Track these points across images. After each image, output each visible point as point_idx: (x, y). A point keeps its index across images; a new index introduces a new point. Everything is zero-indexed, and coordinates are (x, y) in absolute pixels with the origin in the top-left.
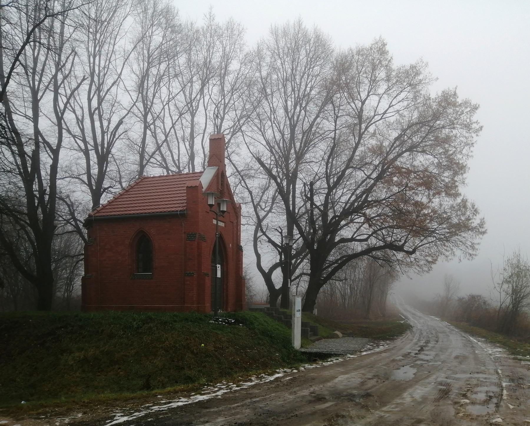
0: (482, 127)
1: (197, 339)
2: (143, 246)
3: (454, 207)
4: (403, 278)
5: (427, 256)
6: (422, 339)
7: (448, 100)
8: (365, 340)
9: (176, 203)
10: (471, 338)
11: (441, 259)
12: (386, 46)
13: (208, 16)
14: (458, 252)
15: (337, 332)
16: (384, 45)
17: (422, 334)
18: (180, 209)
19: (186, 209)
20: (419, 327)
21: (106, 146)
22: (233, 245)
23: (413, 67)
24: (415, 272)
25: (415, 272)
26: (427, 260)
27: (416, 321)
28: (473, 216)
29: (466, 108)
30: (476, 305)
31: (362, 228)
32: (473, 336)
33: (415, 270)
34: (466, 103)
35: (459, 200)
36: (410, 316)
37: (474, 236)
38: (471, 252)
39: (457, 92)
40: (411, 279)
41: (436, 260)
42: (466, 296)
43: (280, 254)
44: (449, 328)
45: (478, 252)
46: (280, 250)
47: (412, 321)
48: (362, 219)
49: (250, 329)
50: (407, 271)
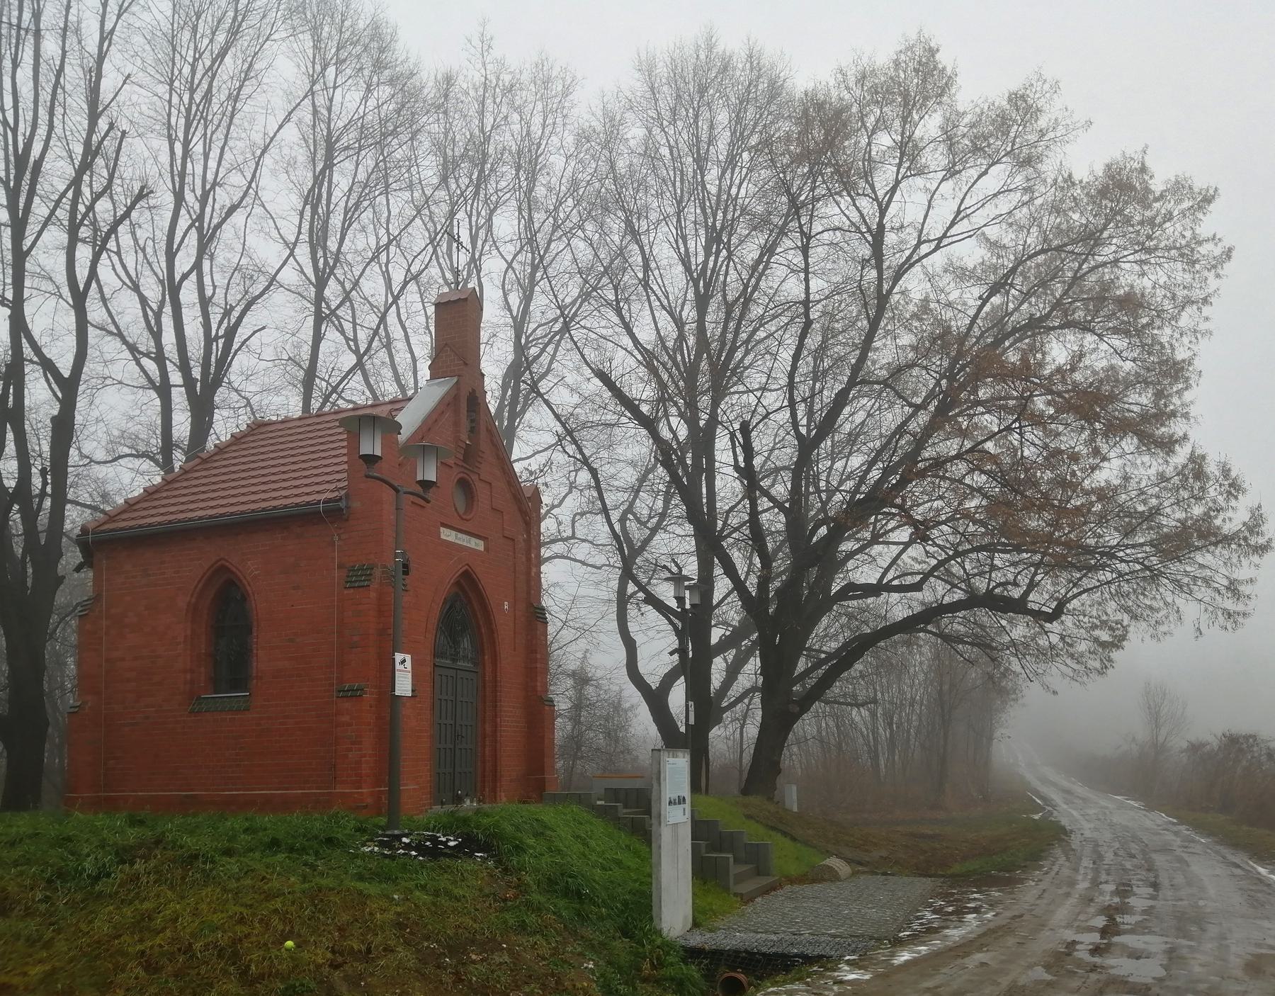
0: (1230, 250)
1: (275, 921)
2: (227, 614)
3: (1168, 480)
4: (1032, 693)
5: (1094, 627)
6: (1103, 877)
7: (1121, 188)
8: (922, 885)
9: (322, 482)
10: (1261, 870)
11: (1137, 634)
12: (938, 56)
13: (476, 42)
14: (1190, 610)
15: (834, 862)
16: (932, 52)
17: (1101, 857)
18: (323, 497)
19: (347, 495)
20: (1088, 834)
21: (212, 370)
22: (513, 606)
23: (1017, 99)
24: (1064, 675)
25: (1064, 675)
26: (1096, 640)
27: (1075, 813)
28: (1227, 500)
29: (1180, 201)
30: (1244, 763)
31: (904, 556)
32: (1261, 860)
33: (1063, 668)
34: (1178, 188)
35: (1181, 455)
36: (1056, 797)
37: (1235, 560)
38: (1229, 604)
39: (1147, 164)
40: (1055, 693)
41: (1123, 638)
42: (1210, 739)
43: (678, 633)
44: (1176, 834)
45: (1251, 604)
46: (680, 625)
47: (1066, 814)
48: (904, 534)
49: (506, 870)
50: (1040, 671)
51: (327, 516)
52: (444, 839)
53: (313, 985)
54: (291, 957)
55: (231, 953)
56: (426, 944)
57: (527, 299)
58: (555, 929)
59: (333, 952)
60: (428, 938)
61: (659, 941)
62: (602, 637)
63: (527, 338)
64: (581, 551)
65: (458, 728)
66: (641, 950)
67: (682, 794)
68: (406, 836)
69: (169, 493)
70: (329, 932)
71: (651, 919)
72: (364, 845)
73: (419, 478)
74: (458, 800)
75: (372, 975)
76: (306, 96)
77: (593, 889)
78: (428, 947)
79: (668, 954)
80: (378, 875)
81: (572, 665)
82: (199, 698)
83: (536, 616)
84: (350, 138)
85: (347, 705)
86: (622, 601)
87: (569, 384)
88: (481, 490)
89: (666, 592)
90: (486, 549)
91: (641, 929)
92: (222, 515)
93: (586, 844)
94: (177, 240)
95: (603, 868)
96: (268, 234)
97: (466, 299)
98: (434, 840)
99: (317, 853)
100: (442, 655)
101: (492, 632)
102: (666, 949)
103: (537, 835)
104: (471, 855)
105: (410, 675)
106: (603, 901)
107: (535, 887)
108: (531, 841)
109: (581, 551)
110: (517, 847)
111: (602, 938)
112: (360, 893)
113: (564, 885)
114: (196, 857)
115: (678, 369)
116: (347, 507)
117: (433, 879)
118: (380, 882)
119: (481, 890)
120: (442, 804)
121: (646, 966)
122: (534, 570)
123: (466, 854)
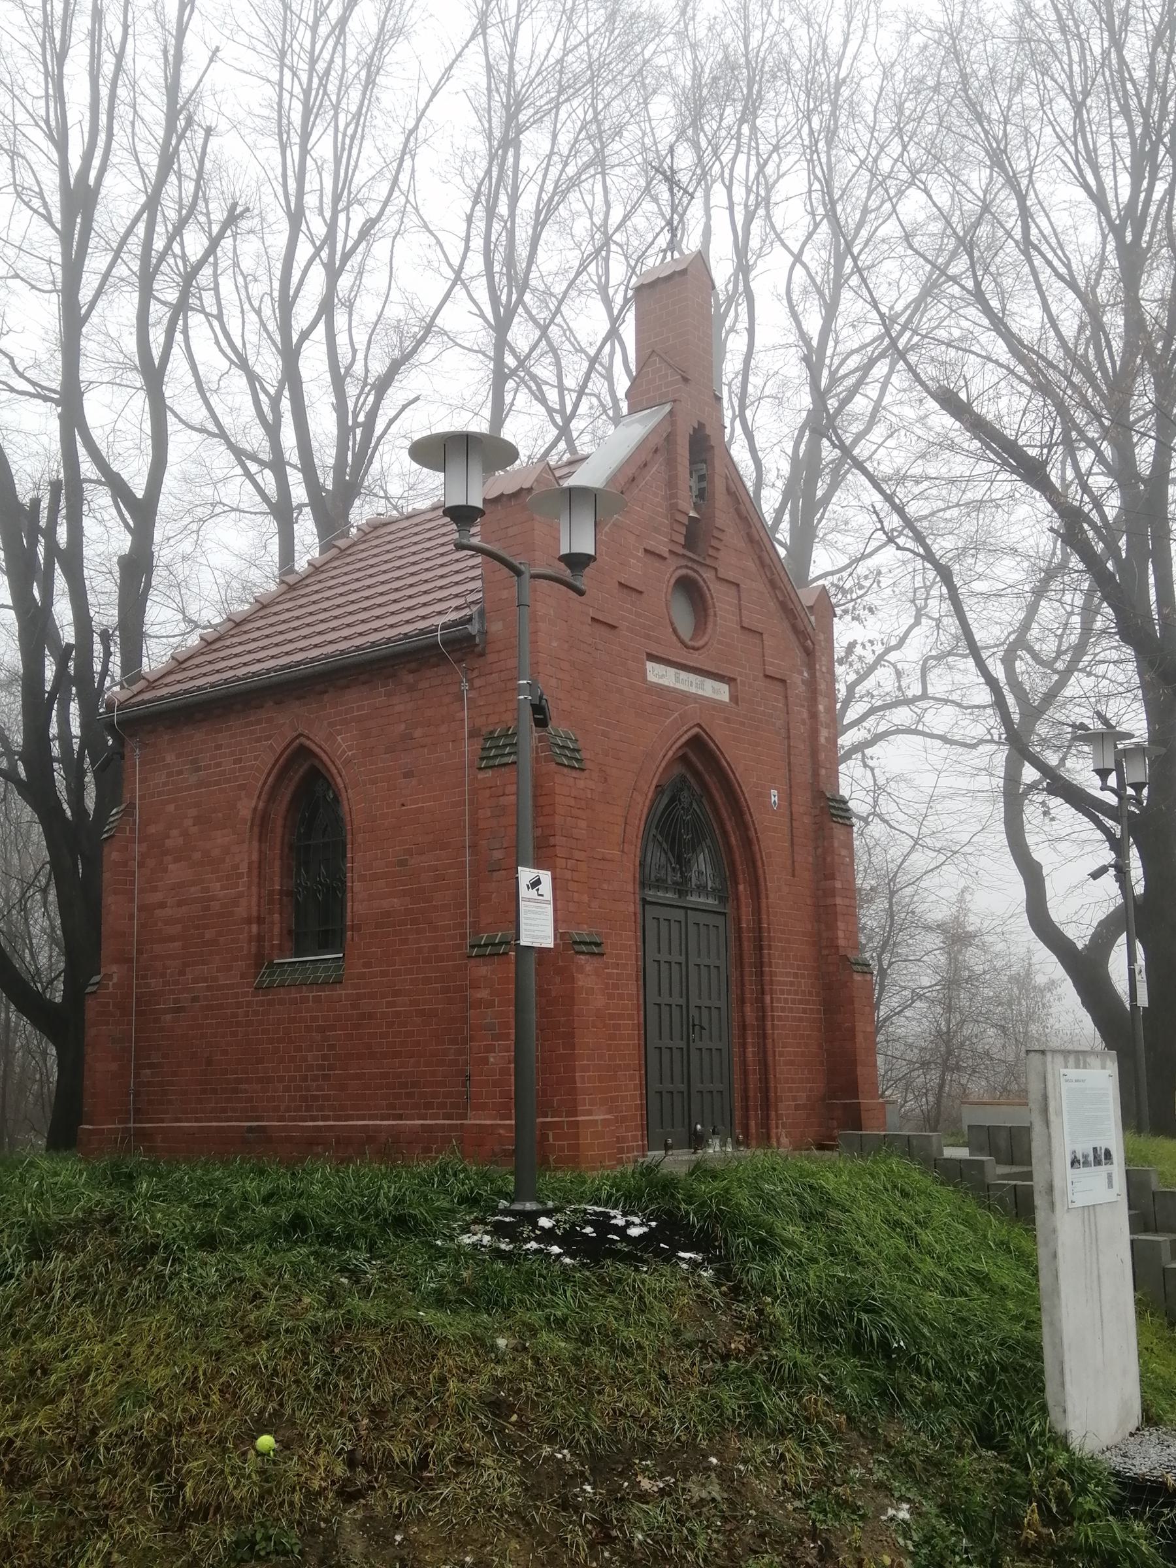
18: (440, 621)
19: (482, 613)
22: (789, 796)
46: (1117, 830)
51: (454, 649)
52: (620, 1222)
53: (292, 1540)
54: (262, 1472)
55: (157, 1457)
56: (546, 1450)
57: (831, 310)
58: (828, 1426)
59: (351, 1463)
60: (551, 1438)
61: (1061, 1461)
62: (984, 862)
63: (832, 374)
64: (940, 719)
65: (693, 1012)
66: (1021, 1478)
67: (1102, 1144)
68: (548, 1214)
69: (235, 640)
70: (352, 1419)
71: (1044, 1409)
72: (466, 1230)
73: (564, 550)
74: (696, 1141)
75: (422, 1518)
76: (473, 38)
77: (915, 1337)
78: (551, 1457)
79: (1084, 1491)
80: (473, 1294)
81: (939, 914)
82: (271, 965)
83: (832, 813)
84: (542, 95)
85: (483, 970)
86: (1014, 798)
87: (900, 430)
88: (721, 599)
89: (1082, 770)
90: (734, 698)
91: (1023, 1430)
92: (299, 663)
93: (912, 1239)
94: (295, 280)
95: (948, 1290)
96: (438, 271)
97: (684, 272)
98: (603, 1224)
99: (371, 1248)
100: (660, 884)
101: (748, 843)
102: (1077, 1477)
103: (810, 1218)
104: (669, 1257)
105: (550, 908)
106: (938, 1365)
107: (790, 1330)
108: (793, 1231)
109: (940, 719)
110: (762, 1242)
111: (932, 1449)
112: (427, 1332)
113: (849, 1327)
114: (152, 1249)
115: (1097, 389)
116: (483, 633)
117: (582, 1307)
118: (476, 1310)
119: (677, 1333)
120: (667, 1147)
121: (1031, 1514)
122: (824, 733)
123: (658, 1253)
